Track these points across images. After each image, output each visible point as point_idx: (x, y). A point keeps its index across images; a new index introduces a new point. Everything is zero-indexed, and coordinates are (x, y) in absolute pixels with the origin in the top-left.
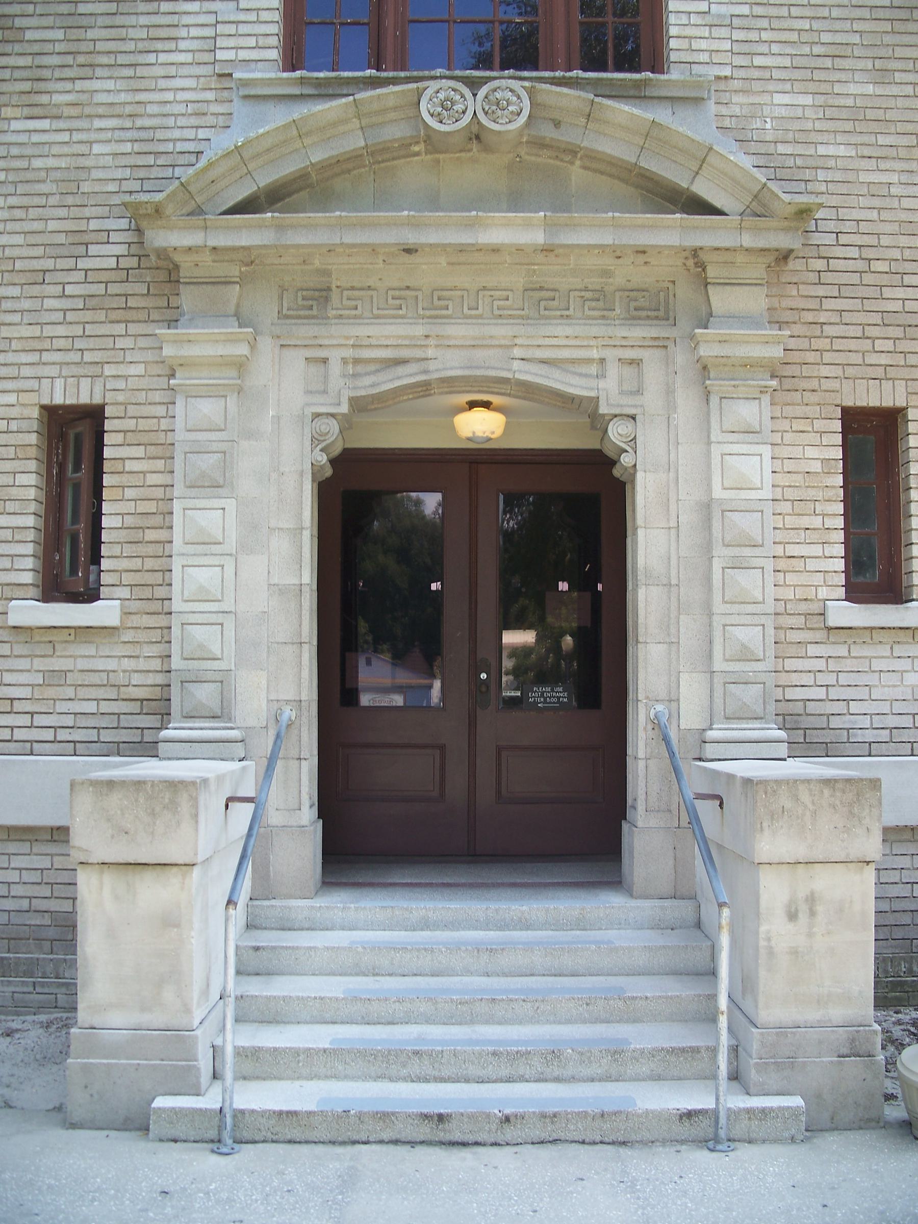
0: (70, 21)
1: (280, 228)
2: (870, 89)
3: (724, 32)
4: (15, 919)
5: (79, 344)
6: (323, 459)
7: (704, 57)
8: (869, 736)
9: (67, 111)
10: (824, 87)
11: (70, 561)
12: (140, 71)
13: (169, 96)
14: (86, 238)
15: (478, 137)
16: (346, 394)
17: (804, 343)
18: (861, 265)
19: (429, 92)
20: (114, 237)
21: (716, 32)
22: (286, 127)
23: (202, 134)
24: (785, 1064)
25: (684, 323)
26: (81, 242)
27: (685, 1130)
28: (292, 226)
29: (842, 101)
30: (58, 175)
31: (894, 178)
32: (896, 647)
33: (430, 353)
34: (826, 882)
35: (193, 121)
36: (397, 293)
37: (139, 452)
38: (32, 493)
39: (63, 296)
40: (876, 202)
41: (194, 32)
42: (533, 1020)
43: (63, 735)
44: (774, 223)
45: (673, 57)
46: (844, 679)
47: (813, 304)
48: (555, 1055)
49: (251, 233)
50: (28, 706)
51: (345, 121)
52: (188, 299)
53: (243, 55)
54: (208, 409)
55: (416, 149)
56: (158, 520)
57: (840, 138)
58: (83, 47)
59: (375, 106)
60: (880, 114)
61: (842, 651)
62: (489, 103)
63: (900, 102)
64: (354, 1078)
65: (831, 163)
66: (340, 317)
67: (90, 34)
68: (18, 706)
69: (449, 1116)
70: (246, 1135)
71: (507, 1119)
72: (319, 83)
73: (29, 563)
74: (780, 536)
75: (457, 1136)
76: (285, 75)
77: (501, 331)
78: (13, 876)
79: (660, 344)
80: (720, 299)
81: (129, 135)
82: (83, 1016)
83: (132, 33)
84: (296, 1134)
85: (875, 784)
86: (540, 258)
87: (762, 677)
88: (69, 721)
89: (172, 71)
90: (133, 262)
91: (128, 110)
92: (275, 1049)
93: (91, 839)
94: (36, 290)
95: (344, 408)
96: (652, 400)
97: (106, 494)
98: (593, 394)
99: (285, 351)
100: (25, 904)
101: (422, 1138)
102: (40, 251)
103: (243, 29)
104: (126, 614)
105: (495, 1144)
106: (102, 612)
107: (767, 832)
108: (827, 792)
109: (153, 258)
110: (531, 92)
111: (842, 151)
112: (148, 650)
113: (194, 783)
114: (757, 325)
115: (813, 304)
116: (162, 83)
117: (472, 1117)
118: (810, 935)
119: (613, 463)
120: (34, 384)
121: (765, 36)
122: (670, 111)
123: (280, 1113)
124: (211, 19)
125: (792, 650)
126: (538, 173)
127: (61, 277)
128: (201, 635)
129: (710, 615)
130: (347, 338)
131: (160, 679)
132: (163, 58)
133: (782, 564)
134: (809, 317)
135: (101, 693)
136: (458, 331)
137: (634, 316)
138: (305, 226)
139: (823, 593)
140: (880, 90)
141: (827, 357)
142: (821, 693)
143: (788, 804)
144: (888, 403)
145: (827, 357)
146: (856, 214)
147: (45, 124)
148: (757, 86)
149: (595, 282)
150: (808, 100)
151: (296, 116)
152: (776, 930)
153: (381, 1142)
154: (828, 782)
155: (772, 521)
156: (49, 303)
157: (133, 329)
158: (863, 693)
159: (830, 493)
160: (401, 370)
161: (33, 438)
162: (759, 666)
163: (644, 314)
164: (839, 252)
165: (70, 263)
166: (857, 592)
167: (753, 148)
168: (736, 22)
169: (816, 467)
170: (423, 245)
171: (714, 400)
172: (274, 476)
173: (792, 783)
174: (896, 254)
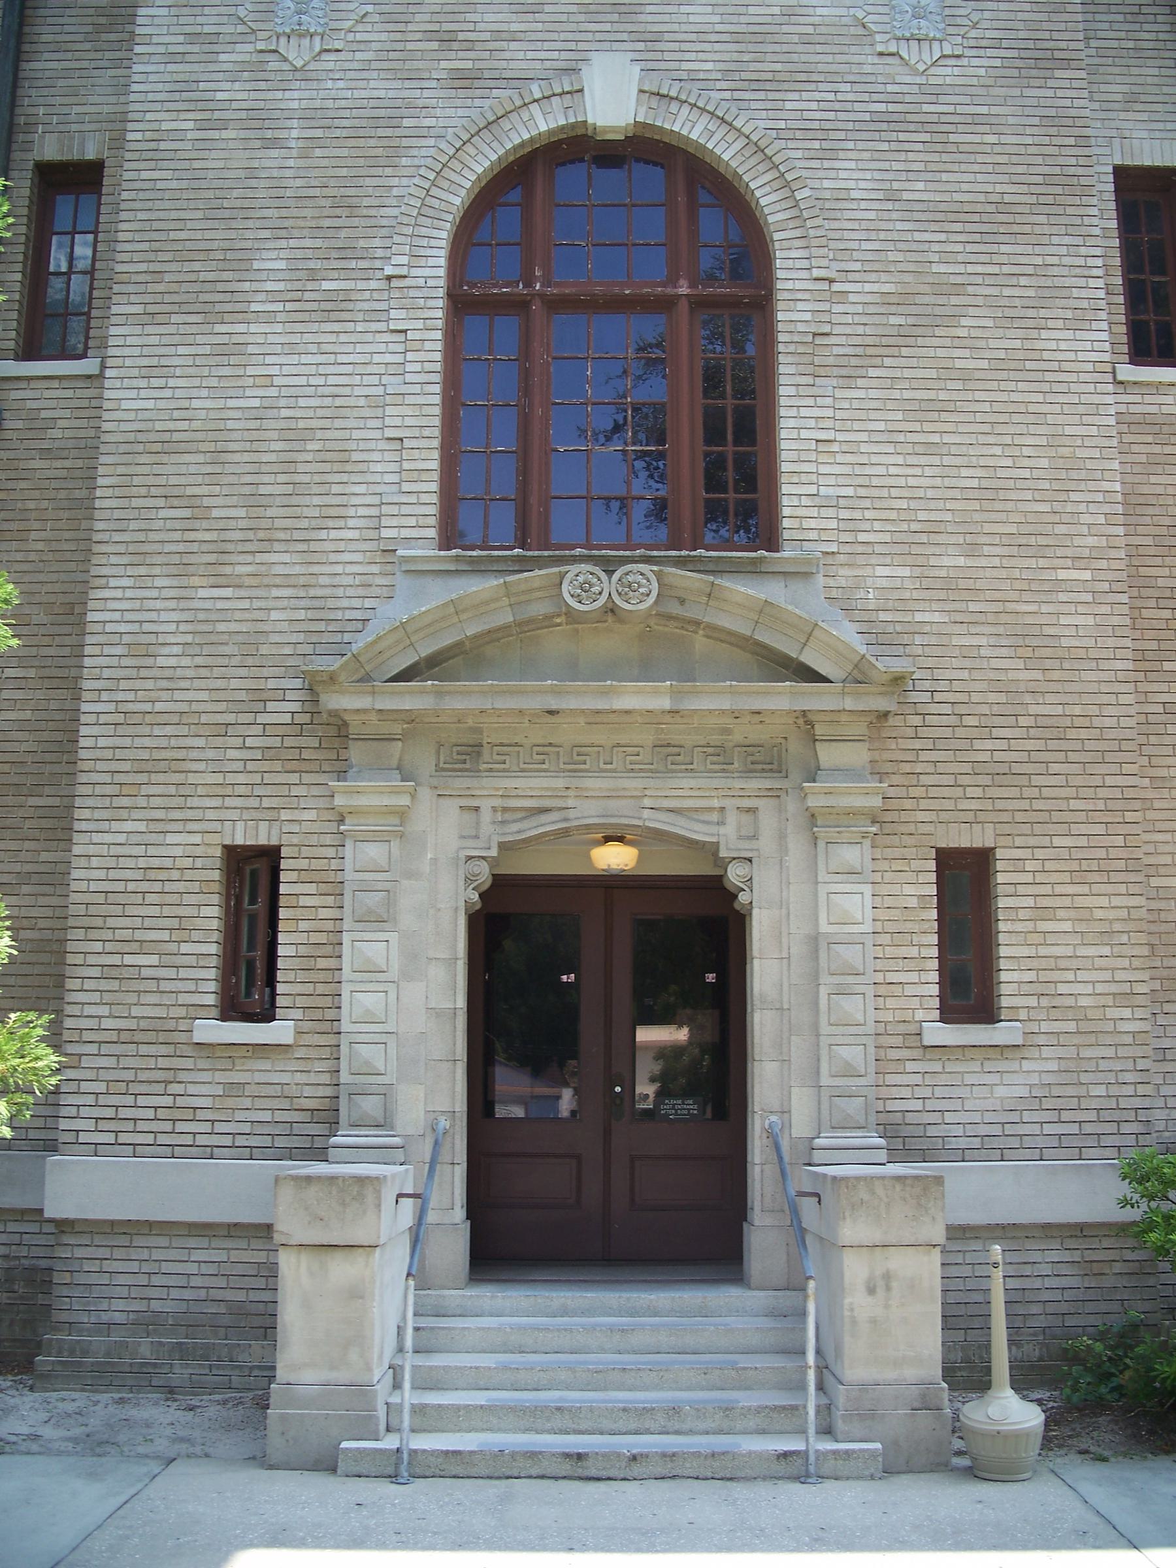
0: (252, 501)
1: (439, 694)
2: (961, 561)
3: (831, 512)
4: (194, 1308)
5: (258, 791)
6: (475, 897)
7: (813, 535)
8: (963, 1143)
9: (248, 581)
10: (921, 561)
11: (249, 986)
12: (314, 546)
13: (339, 569)
14: (264, 696)
15: (612, 611)
16: (496, 839)
17: (901, 792)
18: (953, 720)
19: (569, 576)
20: (290, 695)
21: (825, 512)
22: (445, 605)
23: (368, 603)
24: (867, 1414)
25: (795, 775)
26: (260, 699)
27: (781, 1468)
28: (449, 693)
29: (937, 573)
30: (240, 638)
31: (983, 641)
32: (986, 1063)
33: (570, 803)
34: (903, 1263)
35: (361, 592)
36: (540, 749)
37: (312, 888)
38: (215, 924)
39: (244, 747)
40: (967, 663)
41: (362, 511)
42: (657, 1387)
43: (240, 1141)
44: (872, 689)
45: (786, 535)
46: (939, 1092)
47: (910, 756)
48: (675, 1410)
49: (413, 698)
50: (209, 1115)
51: (497, 600)
52: (356, 753)
53: (405, 533)
54: (374, 852)
55: (558, 620)
56: (328, 950)
57: (935, 606)
58: (264, 524)
59: (523, 587)
60: (970, 584)
61: (937, 1067)
62: (623, 585)
63: (989, 573)
64: (505, 1431)
65: (927, 629)
66: (491, 770)
67: (270, 512)
68: (200, 1115)
69: (587, 1454)
70: (418, 1471)
71: (634, 1458)
72: (472, 560)
73: (212, 986)
74: (880, 965)
75: (593, 1472)
76: (442, 553)
77: (633, 784)
78: (192, 1268)
79: (775, 794)
80: (827, 755)
81: (303, 603)
82: (281, 1374)
83: (307, 512)
84: (460, 1470)
85: (939, 1180)
86: (668, 718)
87: (864, 1091)
88: (246, 1128)
89: (342, 546)
90: (306, 718)
91: (302, 580)
92: (440, 1406)
93: (291, 1225)
94: (219, 741)
95: (494, 852)
96: (766, 844)
97: (281, 926)
98: (714, 840)
99: (441, 800)
100: (202, 1294)
101: (564, 1474)
102: (222, 707)
103: (405, 510)
104: (299, 1033)
105: (624, 1479)
106: (279, 1031)
107: (848, 1220)
108: (898, 1187)
109: (325, 716)
110: (659, 576)
111: (937, 617)
112: (319, 1066)
113: (377, 1178)
114: (860, 778)
115: (910, 756)
116: (333, 557)
117: (604, 1455)
118: (887, 1306)
119: (735, 897)
120: (217, 826)
121: (868, 514)
122: (782, 584)
123: (447, 1452)
124: (375, 500)
125: (892, 1067)
126: (665, 647)
127: (241, 730)
128: (366, 1053)
129: (818, 1035)
130: (498, 789)
131: (329, 1092)
132: (334, 534)
133: (882, 990)
134: (907, 768)
135: (276, 1103)
136: (593, 784)
137: (749, 772)
138: (461, 693)
139: (920, 1015)
140: (970, 562)
141: (923, 804)
142: (918, 1105)
143: (866, 1197)
144: (977, 844)
145: (923, 804)
146: (948, 674)
147: (228, 592)
148: (861, 560)
149: (715, 739)
150: (906, 572)
151: (454, 596)
152: (858, 1302)
153: (530, 1477)
154: (899, 1179)
155: (871, 952)
156: (232, 754)
157: (307, 778)
158: (957, 1105)
159: (926, 926)
160: (544, 818)
161: (216, 875)
162: (862, 1081)
163: (760, 767)
164: (934, 708)
165: (249, 718)
166: (950, 1013)
167: (857, 615)
168: (842, 502)
169: (913, 902)
170: (564, 711)
171: (821, 845)
172: (432, 911)
173: (869, 1180)
174: (985, 709)
